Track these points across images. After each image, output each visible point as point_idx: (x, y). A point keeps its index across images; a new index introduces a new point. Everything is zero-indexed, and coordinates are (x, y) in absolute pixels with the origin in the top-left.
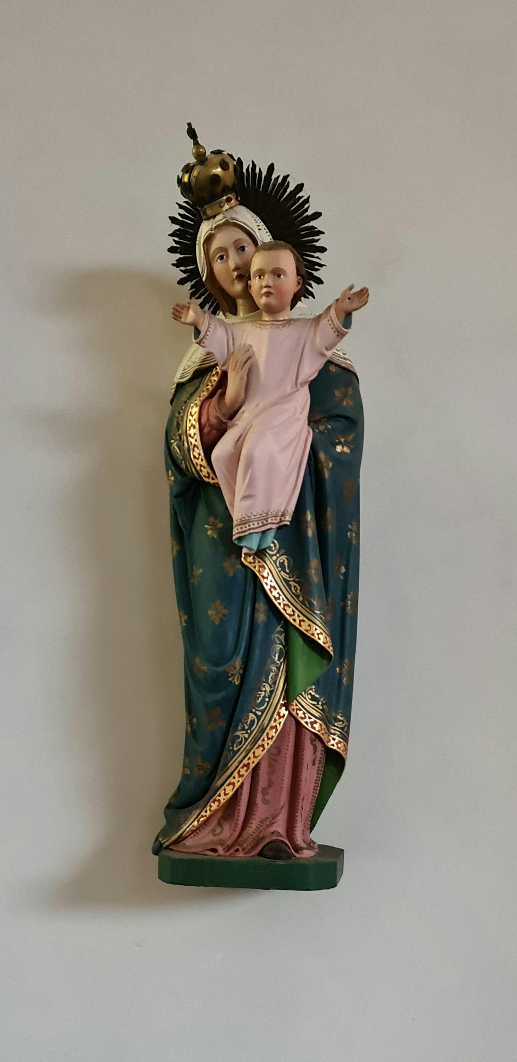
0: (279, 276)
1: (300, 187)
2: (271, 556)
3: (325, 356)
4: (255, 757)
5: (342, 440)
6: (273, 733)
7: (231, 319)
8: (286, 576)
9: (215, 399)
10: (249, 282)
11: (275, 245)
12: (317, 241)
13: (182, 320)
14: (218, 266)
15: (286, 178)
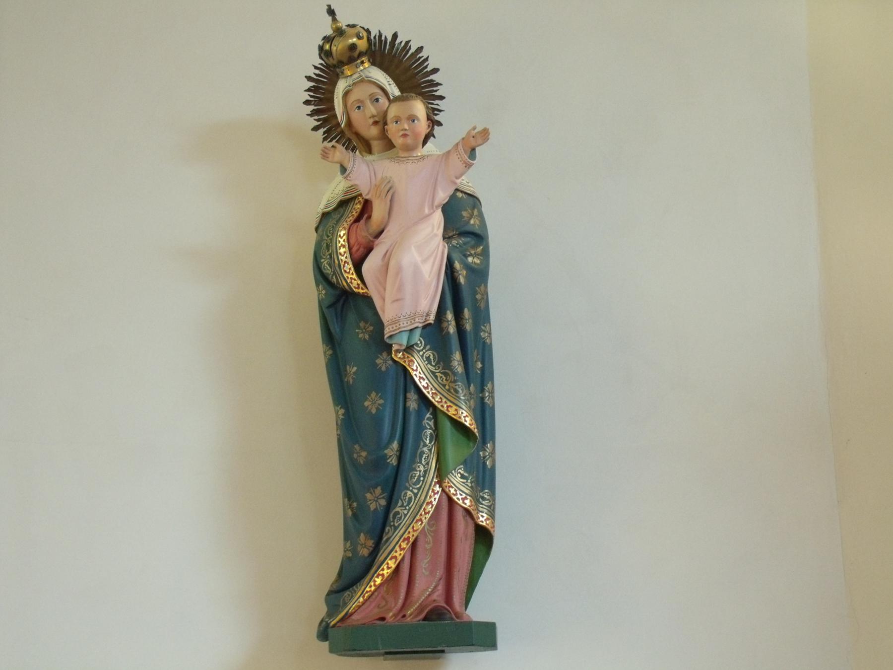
0: (413, 121)
1: (420, 49)
2: (419, 351)
3: (456, 183)
4: (414, 531)
5: (473, 252)
6: (429, 508)
7: (369, 158)
8: (433, 369)
9: (362, 221)
12: (436, 91)
13: (330, 159)
14: (356, 115)
15: (407, 42)
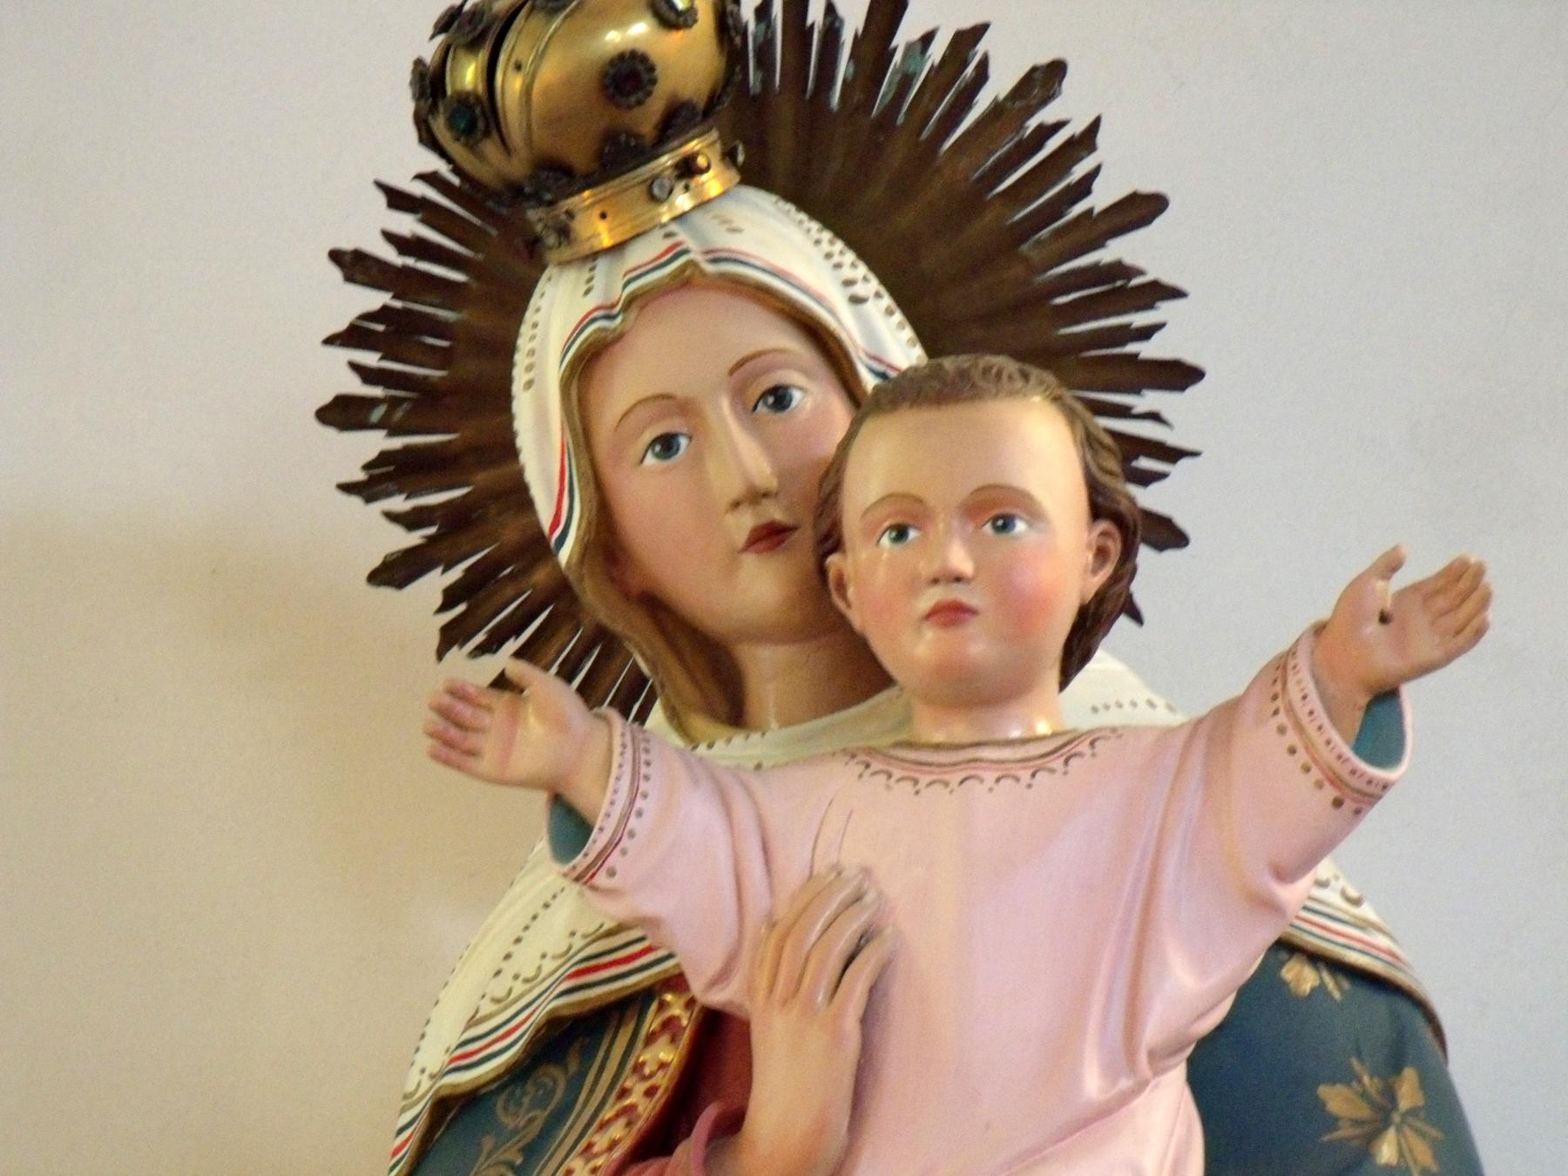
0: (1004, 524)
1: (1046, 79)
10: (833, 560)
11: (935, 373)
12: (1146, 333)
13: (486, 764)
14: (648, 494)
15: (967, 39)
